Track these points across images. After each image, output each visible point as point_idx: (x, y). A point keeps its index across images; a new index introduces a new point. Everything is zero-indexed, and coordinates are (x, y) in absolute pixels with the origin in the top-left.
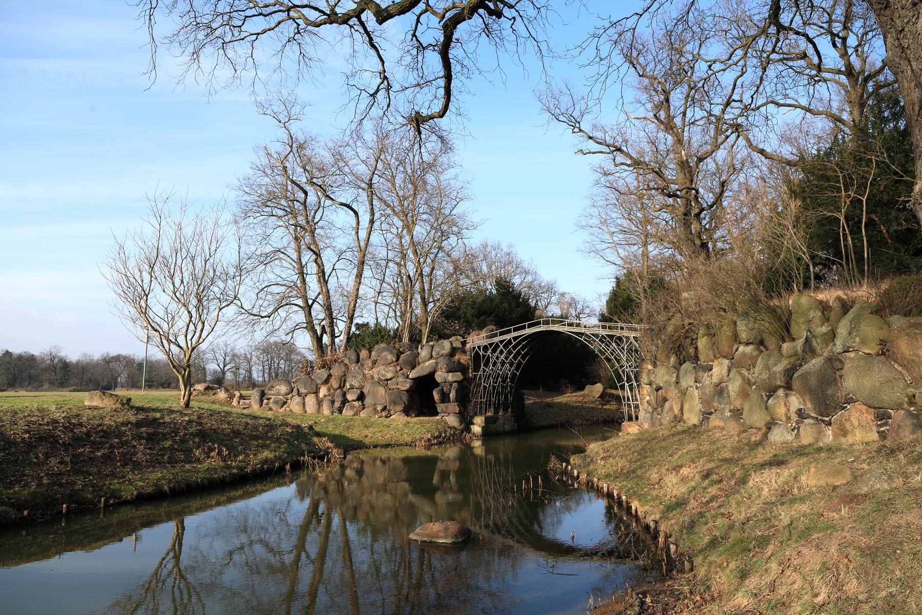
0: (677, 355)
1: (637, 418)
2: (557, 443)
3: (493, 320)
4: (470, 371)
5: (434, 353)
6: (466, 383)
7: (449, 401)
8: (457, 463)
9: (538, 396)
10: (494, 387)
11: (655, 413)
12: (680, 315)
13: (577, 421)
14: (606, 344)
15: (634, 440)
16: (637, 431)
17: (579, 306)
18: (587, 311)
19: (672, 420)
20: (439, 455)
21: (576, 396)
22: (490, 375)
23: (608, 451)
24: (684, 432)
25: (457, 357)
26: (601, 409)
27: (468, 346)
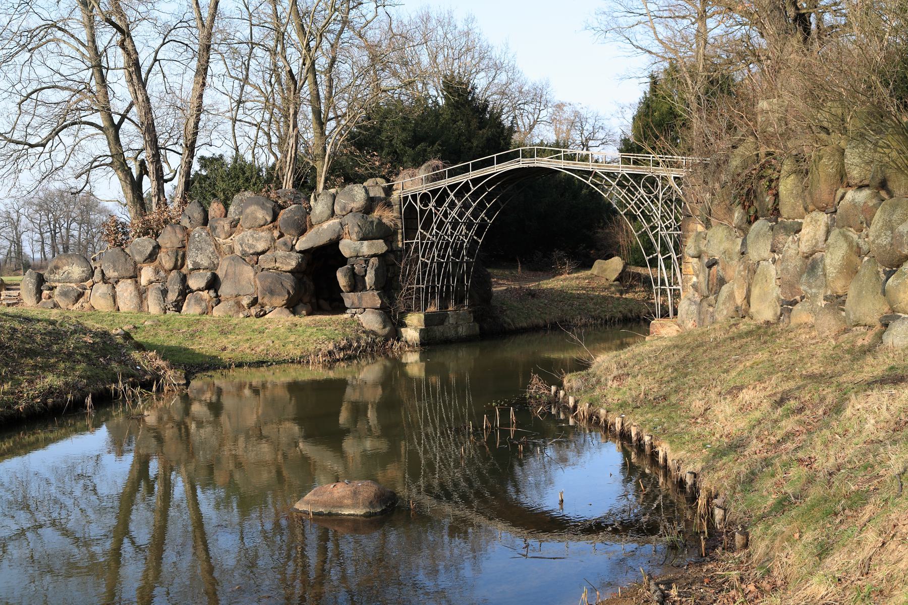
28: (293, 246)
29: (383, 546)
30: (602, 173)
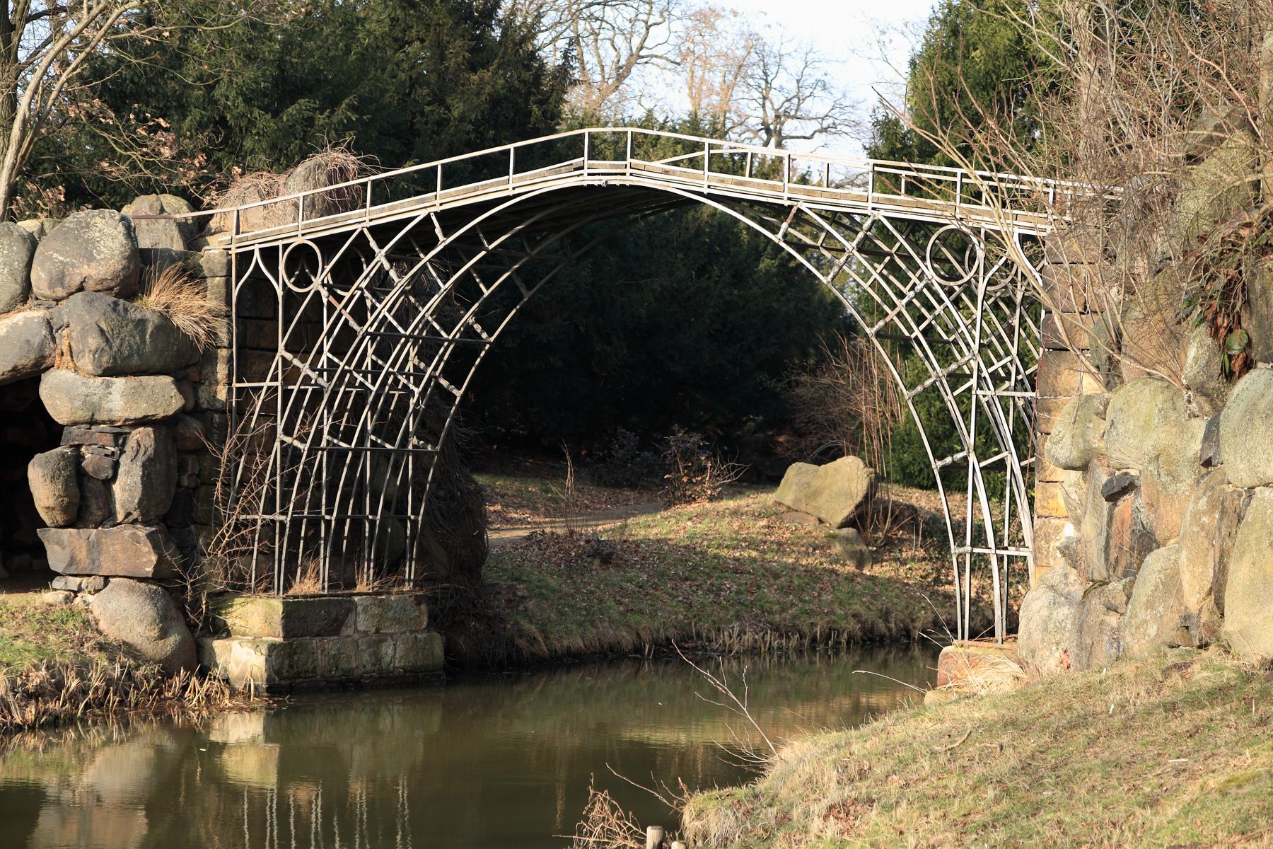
0: (1215, 334)
1: (1012, 628)
2: (636, 734)
3: (347, 126)
4: (221, 371)
5: (39, 278)
6: (195, 428)
7: (108, 517)
8: (140, 823)
9: (556, 508)
10: (337, 457)
11: (1096, 603)
12: (1241, 138)
13: (740, 635)
14: (892, 267)
15: (989, 728)
16: (1008, 687)
17: (784, 82)
18: (817, 105)
19: (1171, 634)
20: (50, 780)
21: (735, 513)
22: (317, 394)
23: (862, 775)
24: (1219, 694)
25: (154, 301)
26: (850, 579)
27: (215, 250)
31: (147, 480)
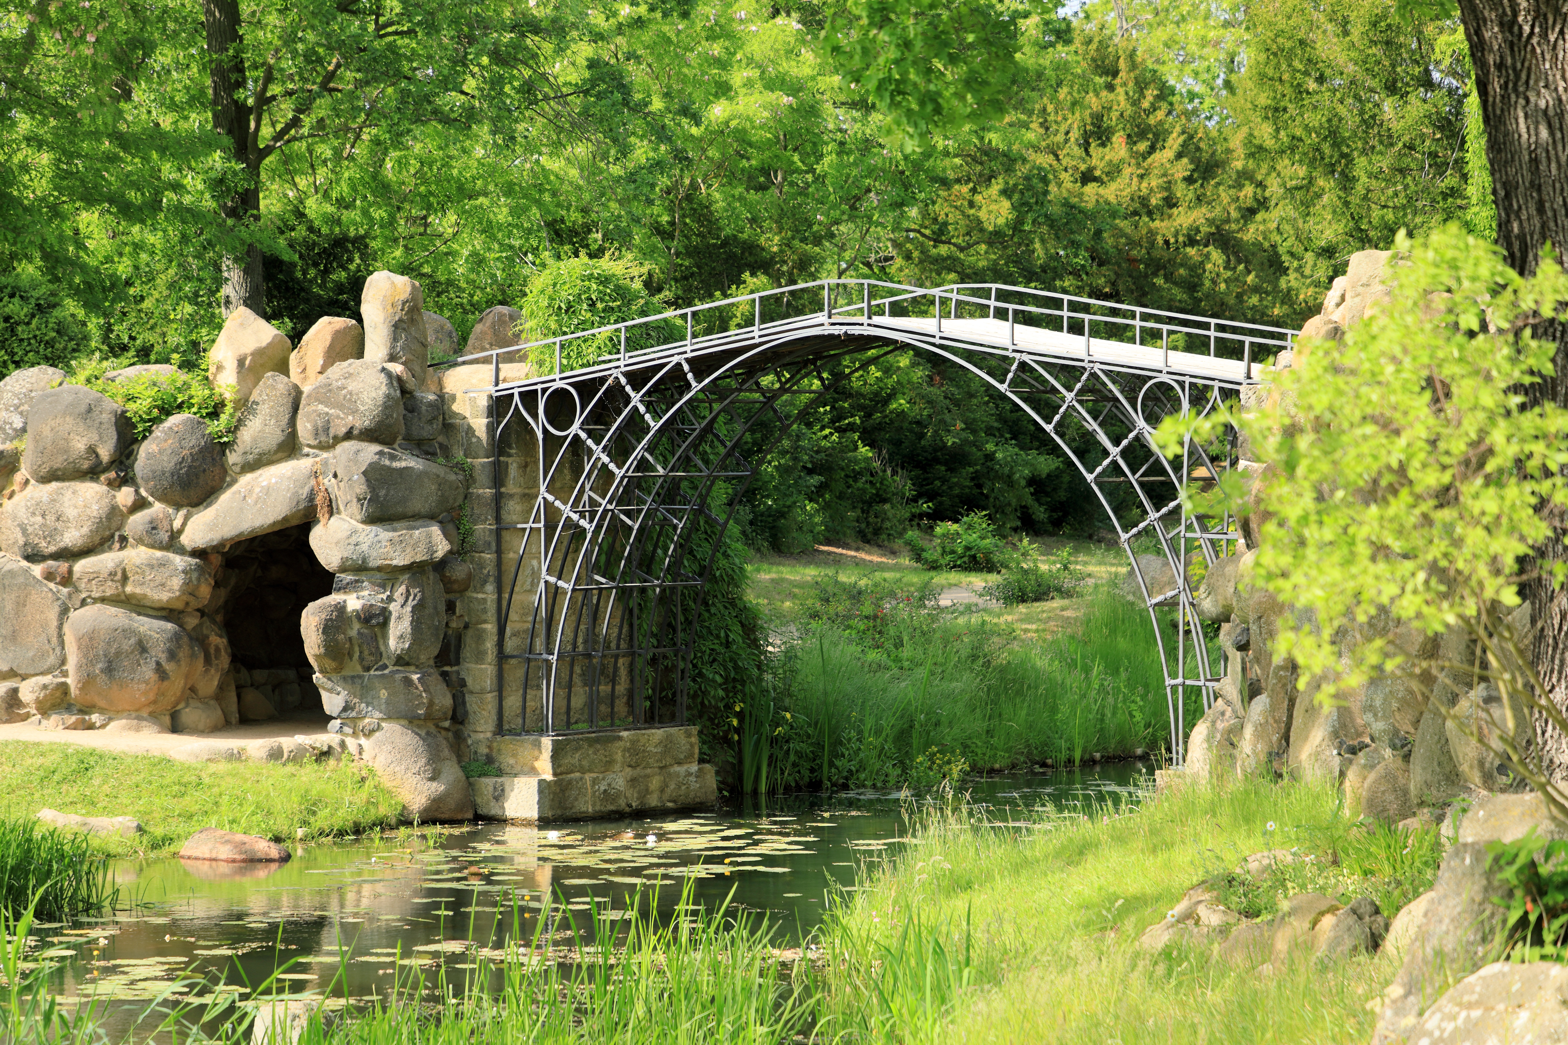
28: (175, 535)
29: (1458, 1013)
30: (1038, 362)
31: (416, 624)
